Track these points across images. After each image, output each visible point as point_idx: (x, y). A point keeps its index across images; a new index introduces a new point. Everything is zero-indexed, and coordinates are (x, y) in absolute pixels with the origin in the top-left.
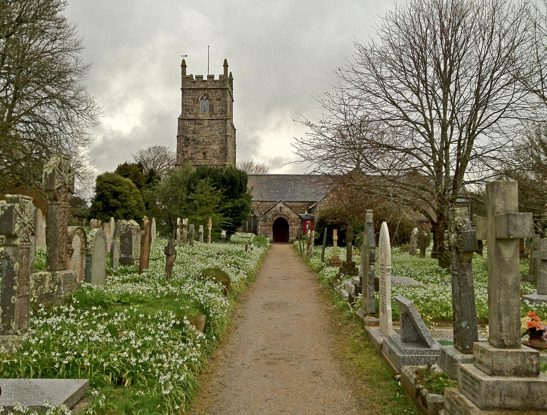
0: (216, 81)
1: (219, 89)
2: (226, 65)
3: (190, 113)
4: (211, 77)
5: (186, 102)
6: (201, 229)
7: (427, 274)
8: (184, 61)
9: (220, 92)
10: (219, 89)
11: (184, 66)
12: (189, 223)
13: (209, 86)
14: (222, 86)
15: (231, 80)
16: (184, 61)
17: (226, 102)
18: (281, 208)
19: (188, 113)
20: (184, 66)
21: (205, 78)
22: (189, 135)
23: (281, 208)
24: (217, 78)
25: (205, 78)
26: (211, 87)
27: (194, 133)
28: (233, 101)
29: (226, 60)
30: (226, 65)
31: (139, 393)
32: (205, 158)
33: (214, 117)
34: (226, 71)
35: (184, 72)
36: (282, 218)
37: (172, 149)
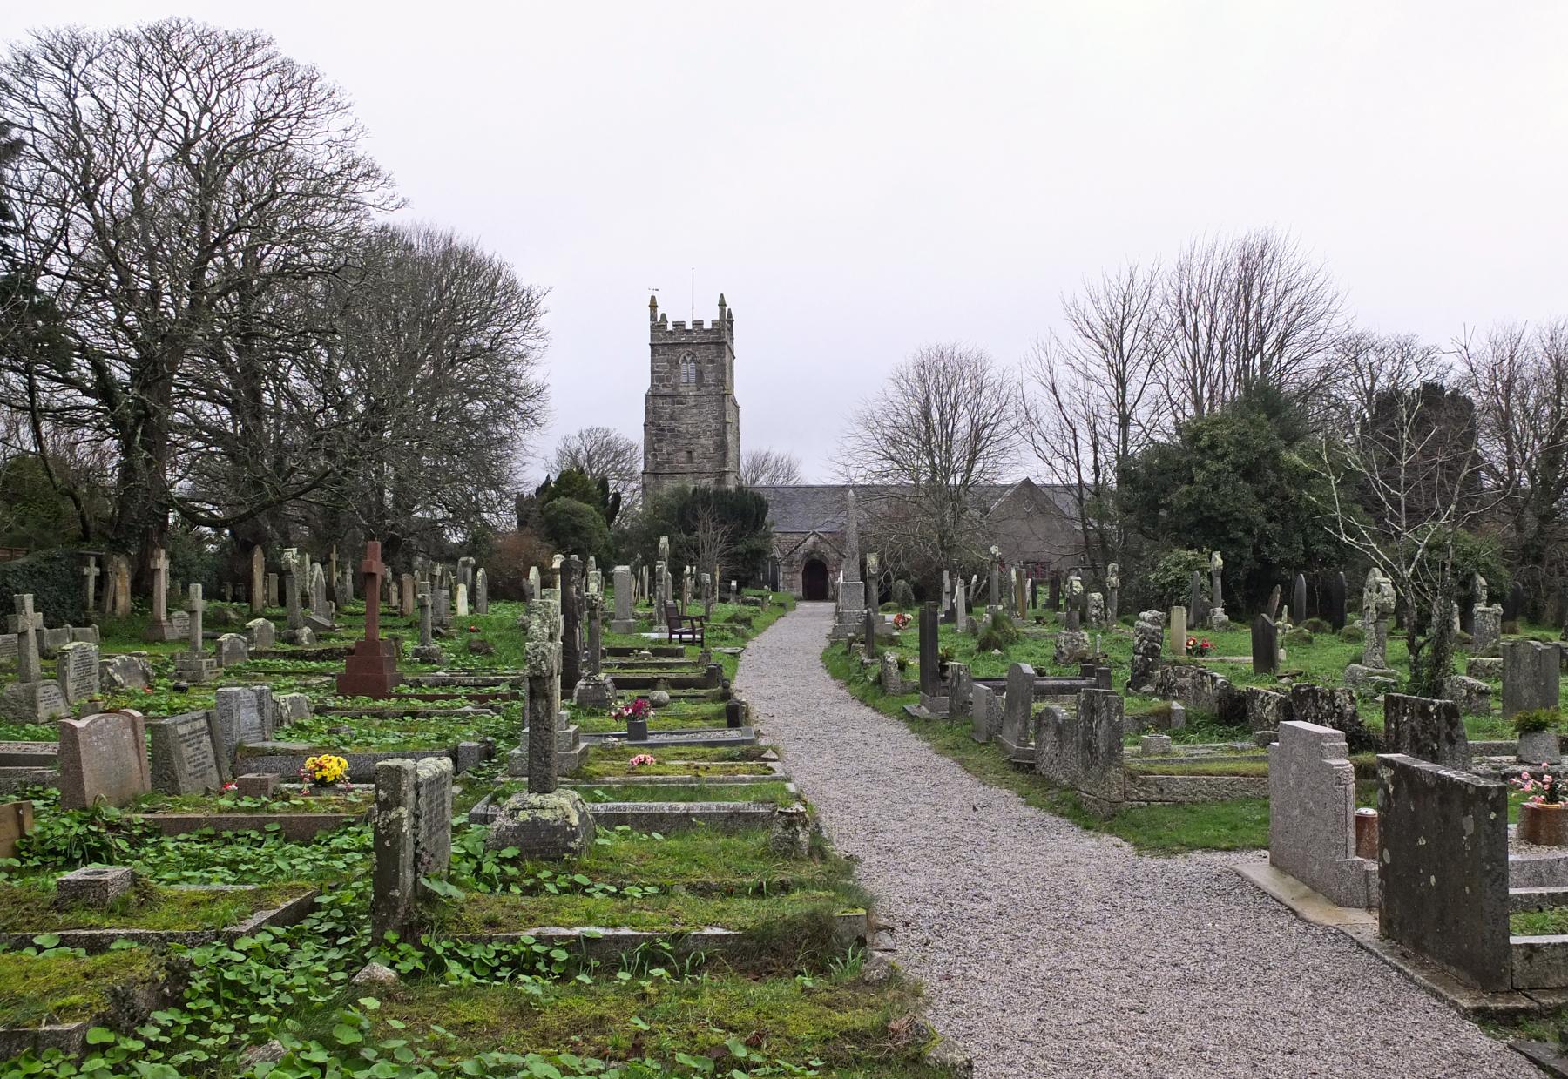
0: (708, 331)
2: (722, 304)
4: (698, 324)
8: (653, 298)
11: (653, 306)
13: (695, 338)
16: (653, 298)
20: (653, 306)
21: (689, 326)
22: (664, 423)
27: (672, 418)
30: (722, 304)
35: (653, 317)
37: (630, 428)
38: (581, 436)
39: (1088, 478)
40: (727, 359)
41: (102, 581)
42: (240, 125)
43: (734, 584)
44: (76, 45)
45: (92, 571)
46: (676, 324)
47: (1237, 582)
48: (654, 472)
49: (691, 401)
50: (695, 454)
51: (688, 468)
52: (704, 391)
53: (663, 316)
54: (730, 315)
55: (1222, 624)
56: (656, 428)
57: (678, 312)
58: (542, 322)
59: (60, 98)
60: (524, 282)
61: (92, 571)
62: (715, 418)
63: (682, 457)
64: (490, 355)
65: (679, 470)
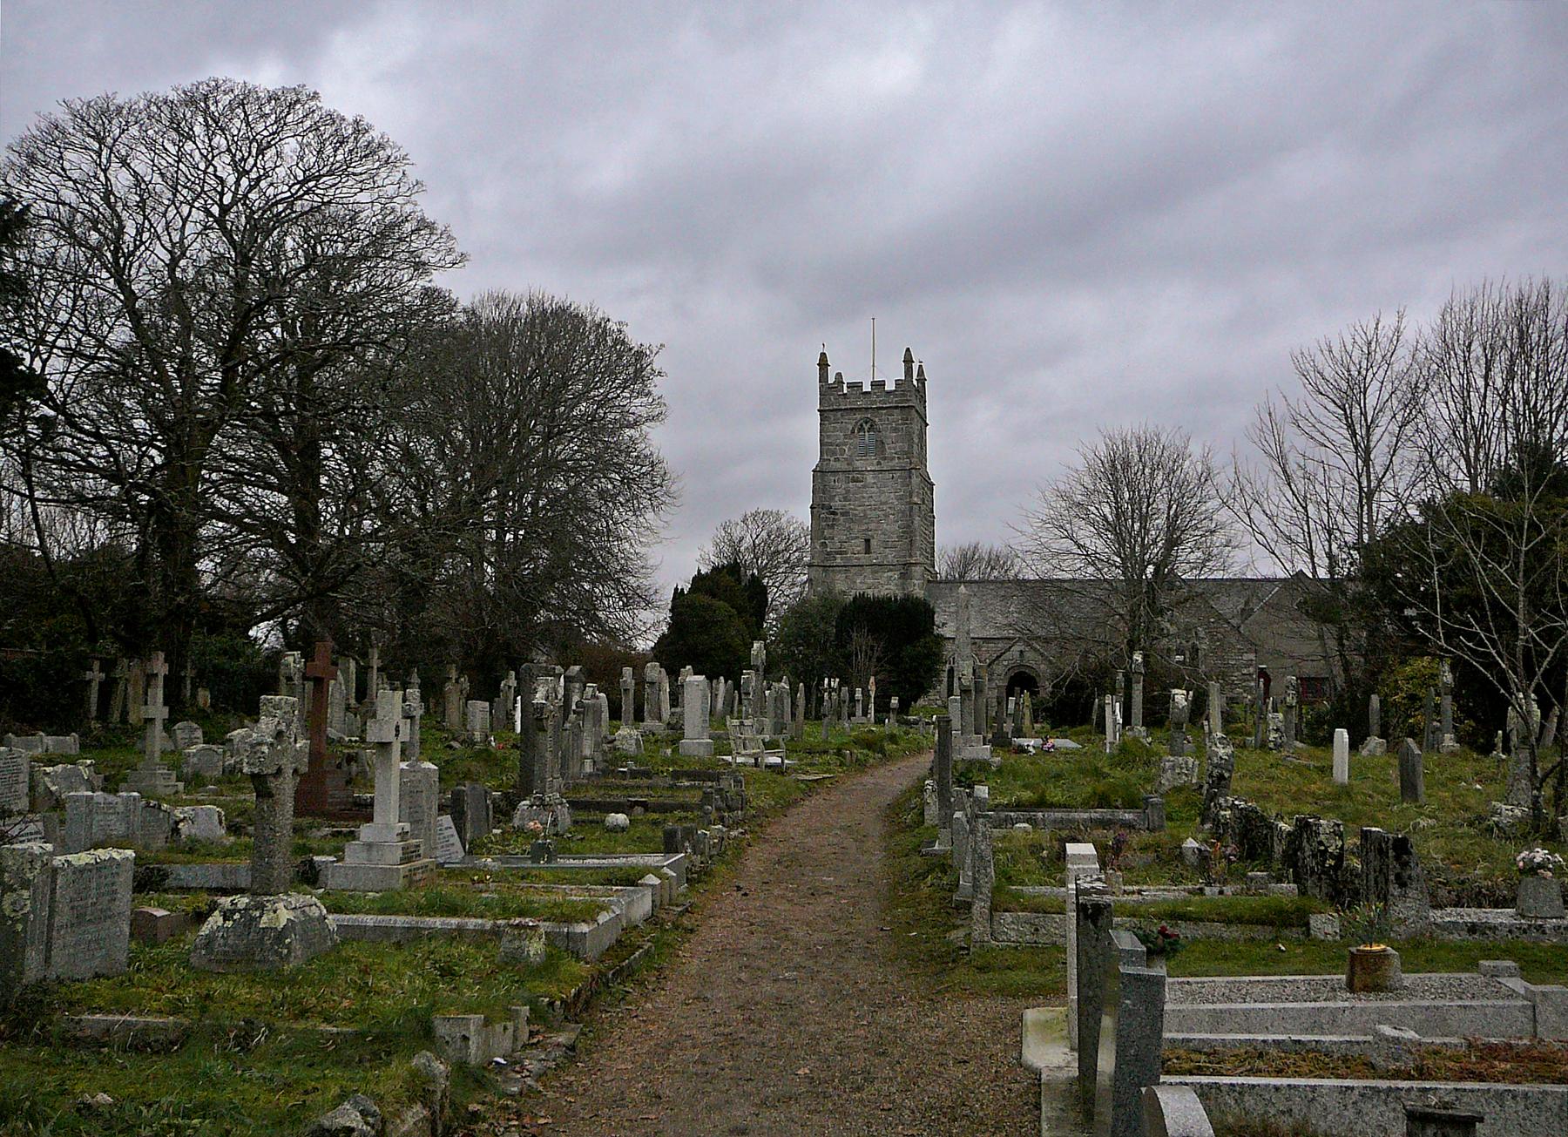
0: (889, 393)
1: (896, 407)
2: (908, 361)
3: (837, 460)
4: (878, 385)
5: (828, 437)
6: (858, 695)
7: (996, 1072)
8: (823, 355)
9: (897, 415)
10: (896, 407)
11: (823, 364)
12: (840, 685)
13: (875, 402)
14: (902, 402)
15: (920, 393)
16: (823, 355)
17: (910, 434)
18: (1021, 652)
19: (832, 459)
20: (823, 364)
21: (867, 388)
22: (837, 503)
23: (1021, 652)
24: (890, 386)
25: (867, 388)
26: (879, 405)
27: (845, 499)
28: (927, 425)
29: (908, 350)
30: (908, 361)
31: (286, 428)
32: (868, 550)
33: (886, 465)
34: (909, 371)
35: (823, 376)
36: (1025, 673)
37: (799, 514)
38: (744, 521)
39: (1323, 573)
40: (916, 427)
41: (107, 688)
42: (279, 184)
43: (895, 701)
44: (106, 112)
45: (96, 675)
46: (850, 386)
47: (1395, 704)
48: (824, 564)
49: (870, 478)
50: (874, 543)
51: (864, 559)
52: (886, 465)
53: (839, 375)
54: (922, 380)
55: (1453, 754)
56: (821, 509)
57: (854, 369)
58: (657, 386)
59: (89, 168)
60: (635, 339)
61: (96, 675)
62: (900, 499)
63: (858, 545)
64: (593, 426)
65: (855, 562)
